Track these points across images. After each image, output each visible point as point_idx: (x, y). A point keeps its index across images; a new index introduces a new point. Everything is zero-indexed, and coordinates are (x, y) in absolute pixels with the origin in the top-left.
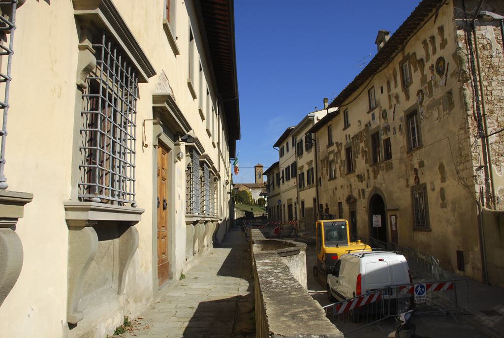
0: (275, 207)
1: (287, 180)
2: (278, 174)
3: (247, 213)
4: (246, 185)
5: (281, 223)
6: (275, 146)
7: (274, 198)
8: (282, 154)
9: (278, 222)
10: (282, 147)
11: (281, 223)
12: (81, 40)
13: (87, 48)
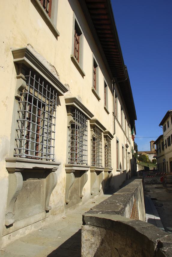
0: (161, 163)
1: (168, 146)
2: (163, 143)
3: (145, 167)
4: (145, 152)
5: (166, 173)
6: (160, 125)
7: (162, 157)
8: (165, 130)
9: (163, 173)
10: (164, 125)
11: (166, 173)
12: (18, 74)
13: (21, 77)
